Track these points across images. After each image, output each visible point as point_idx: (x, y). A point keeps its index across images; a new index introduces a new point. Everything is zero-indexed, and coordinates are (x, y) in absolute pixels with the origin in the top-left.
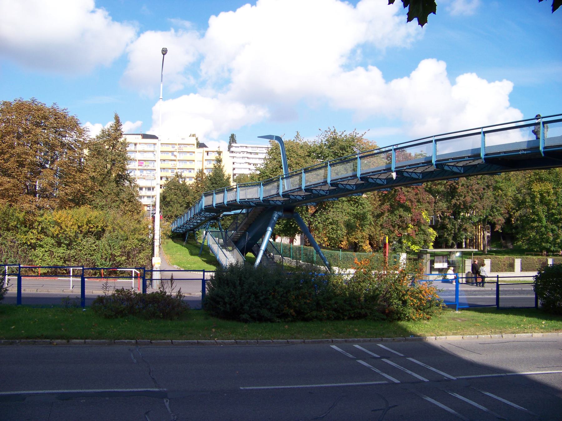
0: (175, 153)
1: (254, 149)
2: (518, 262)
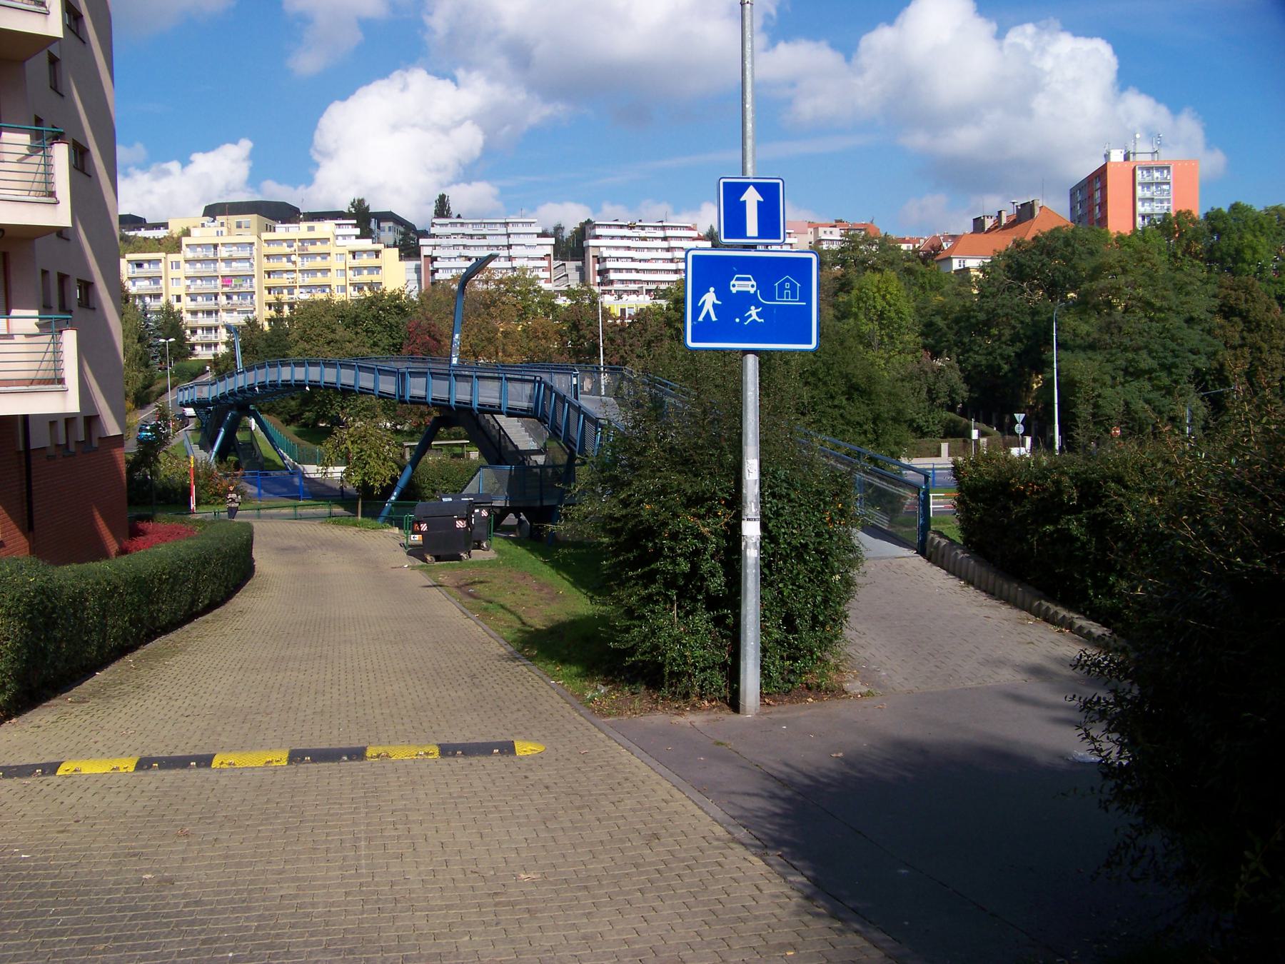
0: (293, 258)
1: (478, 227)
2: (945, 447)
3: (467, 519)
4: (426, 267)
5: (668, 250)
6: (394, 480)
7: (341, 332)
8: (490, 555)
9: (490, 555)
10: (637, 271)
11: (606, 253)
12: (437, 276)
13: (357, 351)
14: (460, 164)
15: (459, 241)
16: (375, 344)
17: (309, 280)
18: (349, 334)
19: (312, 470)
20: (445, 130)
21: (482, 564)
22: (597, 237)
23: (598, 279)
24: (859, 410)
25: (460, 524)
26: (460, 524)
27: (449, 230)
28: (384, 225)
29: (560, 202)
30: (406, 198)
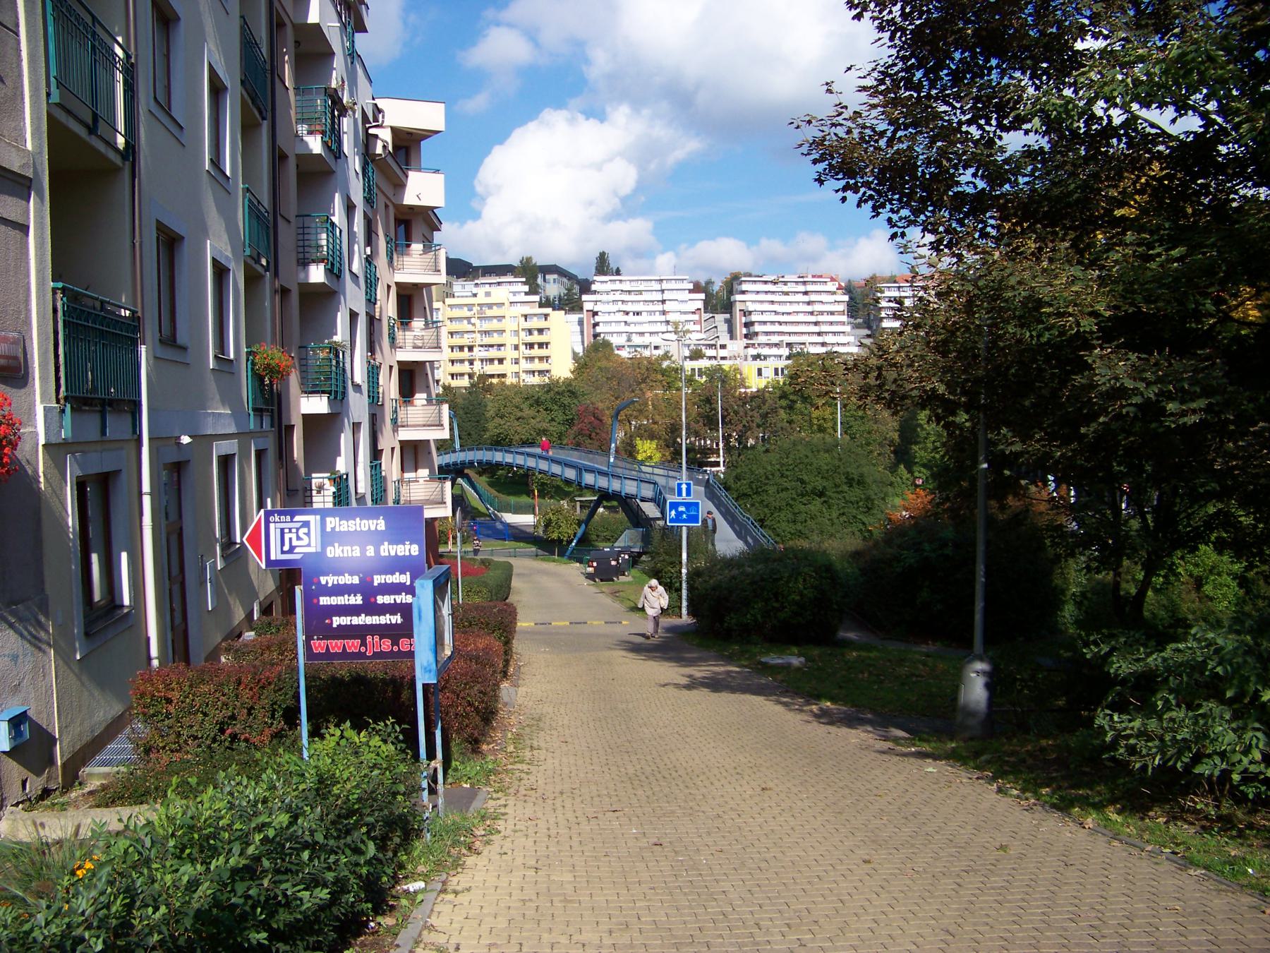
3: (617, 560)
4: (588, 321)
5: (809, 303)
6: (575, 535)
7: (528, 412)
8: (629, 579)
9: (629, 579)
10: (780, 323)
11: (751, 307)
12: (598, 329)
13: (539, 426)
14: (615, 193)
15: (618, 296)
16: (553, 420)
17: (487, 340)
18: (532, 412)
19: (510, 518)
20: (599, 167)
21: (624, 583)
22: (743, 292)
23: (744, 331)
24: (855, 493)
25: (613, 563)
26: (613, 563)
27: (609, 286)
28: (550, 277)
29: (712, 238)
30: (564, 246)
